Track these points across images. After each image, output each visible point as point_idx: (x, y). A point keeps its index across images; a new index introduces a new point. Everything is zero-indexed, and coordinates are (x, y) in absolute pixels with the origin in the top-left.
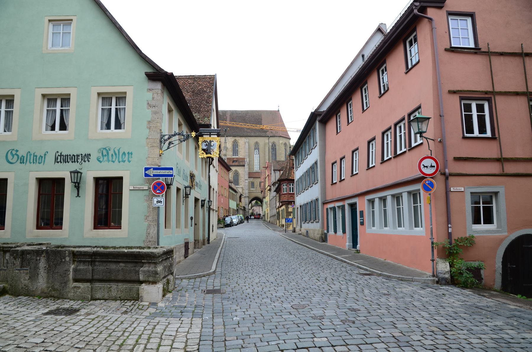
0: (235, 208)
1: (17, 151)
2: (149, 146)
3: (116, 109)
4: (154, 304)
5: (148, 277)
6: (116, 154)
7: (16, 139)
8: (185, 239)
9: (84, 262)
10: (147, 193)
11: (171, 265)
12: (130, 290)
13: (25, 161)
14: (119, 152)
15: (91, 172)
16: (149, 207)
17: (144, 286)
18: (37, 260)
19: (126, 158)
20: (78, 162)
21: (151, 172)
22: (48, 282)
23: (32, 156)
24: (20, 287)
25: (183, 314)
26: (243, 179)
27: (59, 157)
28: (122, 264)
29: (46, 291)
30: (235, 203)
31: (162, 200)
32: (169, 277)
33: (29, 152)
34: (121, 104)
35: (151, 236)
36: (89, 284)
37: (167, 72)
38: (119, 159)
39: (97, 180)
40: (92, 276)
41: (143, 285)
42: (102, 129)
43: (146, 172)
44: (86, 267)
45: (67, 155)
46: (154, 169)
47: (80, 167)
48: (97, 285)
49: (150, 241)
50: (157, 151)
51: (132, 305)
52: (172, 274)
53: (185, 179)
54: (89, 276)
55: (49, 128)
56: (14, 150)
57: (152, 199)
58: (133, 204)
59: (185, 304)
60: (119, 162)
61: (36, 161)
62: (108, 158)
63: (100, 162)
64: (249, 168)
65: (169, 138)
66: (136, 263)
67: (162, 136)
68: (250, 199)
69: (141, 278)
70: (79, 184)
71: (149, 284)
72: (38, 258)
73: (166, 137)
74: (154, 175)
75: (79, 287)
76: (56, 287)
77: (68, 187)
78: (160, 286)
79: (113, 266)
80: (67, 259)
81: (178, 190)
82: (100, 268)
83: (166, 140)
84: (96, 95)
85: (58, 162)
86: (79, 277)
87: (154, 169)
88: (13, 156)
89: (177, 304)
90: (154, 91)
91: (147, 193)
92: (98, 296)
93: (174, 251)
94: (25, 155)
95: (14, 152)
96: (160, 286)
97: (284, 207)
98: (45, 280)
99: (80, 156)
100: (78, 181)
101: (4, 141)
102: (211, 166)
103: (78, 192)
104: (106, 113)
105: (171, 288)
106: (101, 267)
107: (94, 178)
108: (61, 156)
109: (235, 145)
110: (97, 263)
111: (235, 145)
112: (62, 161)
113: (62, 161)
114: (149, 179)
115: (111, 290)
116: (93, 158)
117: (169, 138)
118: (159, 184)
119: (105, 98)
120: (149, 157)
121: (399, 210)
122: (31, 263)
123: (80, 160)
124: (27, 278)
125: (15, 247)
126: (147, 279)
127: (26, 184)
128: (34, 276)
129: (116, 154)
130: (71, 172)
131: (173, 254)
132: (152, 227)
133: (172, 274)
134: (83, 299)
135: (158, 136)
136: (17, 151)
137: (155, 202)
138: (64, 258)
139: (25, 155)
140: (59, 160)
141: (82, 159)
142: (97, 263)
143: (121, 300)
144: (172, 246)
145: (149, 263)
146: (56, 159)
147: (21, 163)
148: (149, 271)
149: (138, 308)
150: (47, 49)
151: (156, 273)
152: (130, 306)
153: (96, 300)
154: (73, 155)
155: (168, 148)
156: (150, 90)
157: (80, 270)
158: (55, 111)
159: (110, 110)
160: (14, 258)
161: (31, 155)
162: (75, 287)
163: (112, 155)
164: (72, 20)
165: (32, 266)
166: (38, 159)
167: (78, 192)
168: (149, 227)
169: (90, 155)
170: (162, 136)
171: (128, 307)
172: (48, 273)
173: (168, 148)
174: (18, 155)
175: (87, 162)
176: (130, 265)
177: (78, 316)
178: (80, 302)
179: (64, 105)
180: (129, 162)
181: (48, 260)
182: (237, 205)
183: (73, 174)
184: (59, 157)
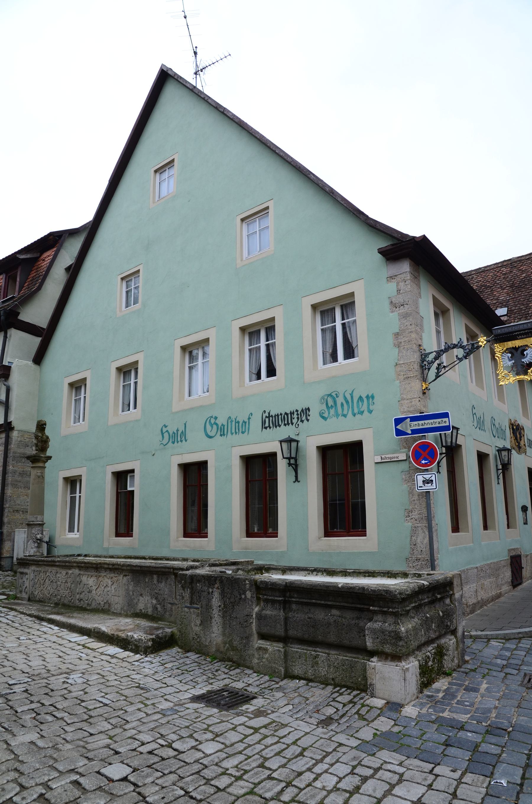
1: (216, 418)
2: (402, 377)
3: (344, 325)
4: (394, 707)
5: (383, 642)
6: (347, 402)
8: (509, 550)
9: (273, 602)
10: (405, 466)
11: (449, 614)
12: (351, 667)
13: (225, 433)
14: (352, 397)
16: (411, 492)
17: (375, 663)
18: (209, 593)
19: (365, 407)
20: (292, 424)
21: (408, 426)
22: (224, 634)
23: (234, 423)
24: (191, 636)
25: (451, 751)
27: (267, 420)
28: (335, 612)
29: (222, 649)
31: (433, 478)
32: (443, 641)
33: (230, 417)
34: (350, 315)
35: (419, 549)
36: (281, 645)
37: (414, 238)
38: (353, 410)
40: (286, 630)
41: (375, 659)
42: (325, 363)
43: (398, 427)
44: (274, 613)
45: (278, 415)
46: (413, 419)
47: (297, 431)
48: (296, 649)
49: (418, 560)
50: (417, 385)
51: (351, 702)
52: (454, 632)
53: (498, 433)
54: (280, 631)
55: (254, 376)
56: (212, 417)
57: (411, 480)
58: (381, 489)
59: (463, 718)
60: (354, 415)
61: (239, 430)
62: (336, 411)
63: (325, 418)
65: (436, 358)
66: (361, 610)
67: (424, 356)
69: (369, 644)
70: (296, 459)
71: (386, 659)
72: (211, 590)
73: (431, 357)
74: (414, 432)
75: (266, 650)
76: (235, 643)
77: (282, 465)
78: (412, 665)
79: (320, 615)
80: (249, 594)
81: (482, 457)
82: (299, 615)
83: (432, 362)
84: (309, 309)
85: (266, 428)
86: (265, 630)
87: (413, 419)
88: (212, 426)
89: (446, 714)
90: (398, 278)
91: (405, 466)
92: (297, 670)
93: (455, 583)
94: (225, 424)
95: (213, 421)
96: (412, 665)
98: (221, 629)
99: (295, 413)
100: (293, 455)
101: (201, 406)
104: (329, 336)
105: (448, 663)
106: (299, 615)
107: (318, 447)
108: (269, 417)
112: (271, 425)
113: (271, 425)
114: (406, 440)
115: (317, 663)
116: (314, 414)
117: (436, 358)
118: (426, 446)
119: (324, 311)
120: (403, 399)
121: (73, 500)
122: (202, 598)
123: (295, 421)
124: (198, 622)
125: (187, 569)
126: (380, 648)
127: (229, 467)
128: (206, 621)
129: (347, 402)
130: (281, 442)
131: (452, 589)
132: (420, 532)
133: (454, 632)
134: (272, 674)
135: (416, 358)
136: (216, 418)
137: (420, 483)
138: (244, 593)
140: (267, 425)
141: (298, 418)
142: (294, 606)
143: (335, 686)
144: (450, 574)
145: (384, 613)
146: (263, 423)
147: (221, 435)
148: (383, 631)
149: (357, 713)
150: (242, 260)
151: (397, 637)
152: (344, 705)
153: (293, 677)
154: (286, 414)
155: (438, 376)
156: (391, 278)
157: (265, 617)
158: (259, 348)
159: (334, 329)
160: (182, 586)
161: (232, 421)
162: (260, 648)
163: (342, 405)
164: (267, 208)
165: (204, 603)
166: (241, 427)
168: (414, 531)
169: (309, 409)
170: (424, 356)
171: (340, 706)
172: (223, 617)
173: (438, 376)
174: (217, 424)
175: (305, 421)
176: (349, 615)
177: (238, 715)
178: (267, 678)
179: (270, 337)
180: (370, 412)
181: (223, 595)
183: (285, 445)
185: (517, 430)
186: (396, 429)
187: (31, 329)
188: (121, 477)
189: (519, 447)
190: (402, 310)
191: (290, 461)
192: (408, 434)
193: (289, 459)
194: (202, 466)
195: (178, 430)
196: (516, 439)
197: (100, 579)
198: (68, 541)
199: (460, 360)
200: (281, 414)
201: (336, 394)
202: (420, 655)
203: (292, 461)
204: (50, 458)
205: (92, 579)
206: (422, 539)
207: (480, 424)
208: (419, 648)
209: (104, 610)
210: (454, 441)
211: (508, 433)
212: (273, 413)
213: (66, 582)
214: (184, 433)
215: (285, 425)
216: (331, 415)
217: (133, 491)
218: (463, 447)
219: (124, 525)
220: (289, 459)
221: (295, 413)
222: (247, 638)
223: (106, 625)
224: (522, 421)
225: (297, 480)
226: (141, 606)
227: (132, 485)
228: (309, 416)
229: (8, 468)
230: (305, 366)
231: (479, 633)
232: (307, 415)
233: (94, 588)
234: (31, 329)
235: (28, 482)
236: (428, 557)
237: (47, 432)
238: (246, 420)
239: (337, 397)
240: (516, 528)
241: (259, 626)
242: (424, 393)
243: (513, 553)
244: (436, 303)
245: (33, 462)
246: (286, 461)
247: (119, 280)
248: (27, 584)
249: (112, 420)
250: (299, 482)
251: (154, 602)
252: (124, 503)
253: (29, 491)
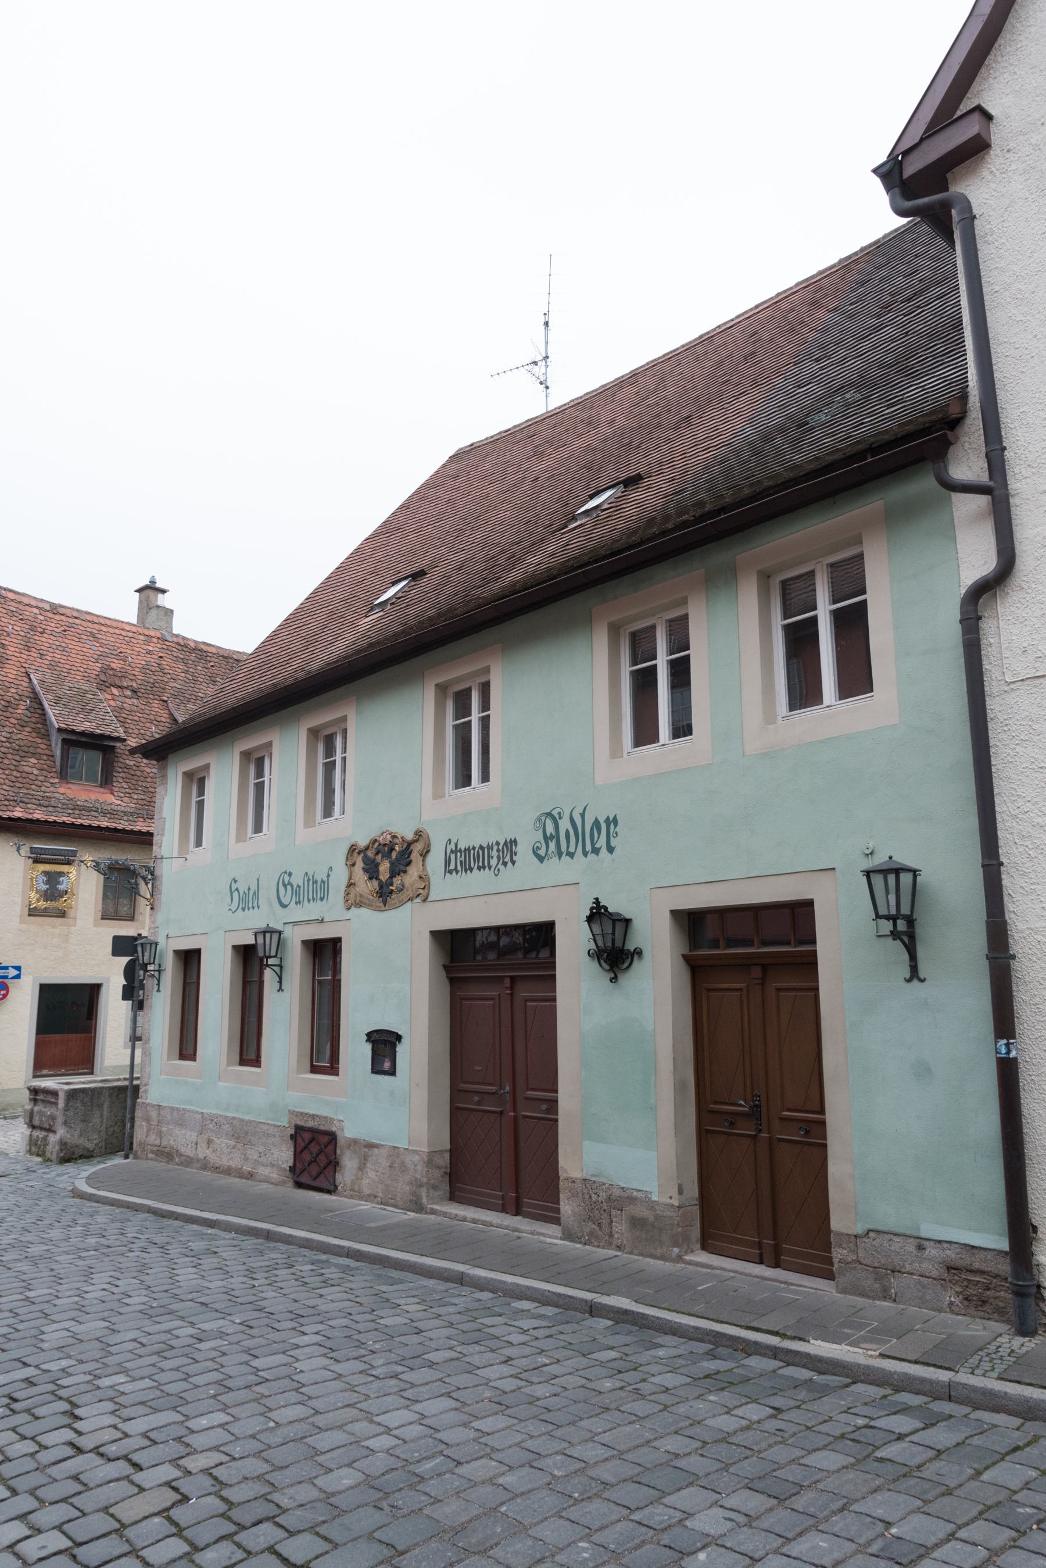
1: (290, 874)
27: (453, 856)
63: (541, 859)
70: (910, 921)
85: (450, 872)
88: (285, 886)
95: (287, 878)
99: (495, 848)
100: (905, 910)
112: (459, 868)
113: (459, 868)
116: (523, 850)
123: (494, 862)
140: (452, 867)
141: (499, 858)
146: (447, 862)
154: (481, 847)
163: (567, 832)
174: (290, 883)
175: (510, 864)
183: (878, 880)
184: (453, 856)
191: (895, 925)
193: (894, 919)
195: (249, 889)
200: (474, 848)
201: (559, 813)
203: (902, 925)
204: (615, 816)
215: (479, 868)
216: (550, 852)
220: (894, 919)
221: (495, 848)
225: (914, 974)
228: (516, 854)
232: (513, 854)
238: (325, 879)
239: (560, 818)
250: (923, 981)
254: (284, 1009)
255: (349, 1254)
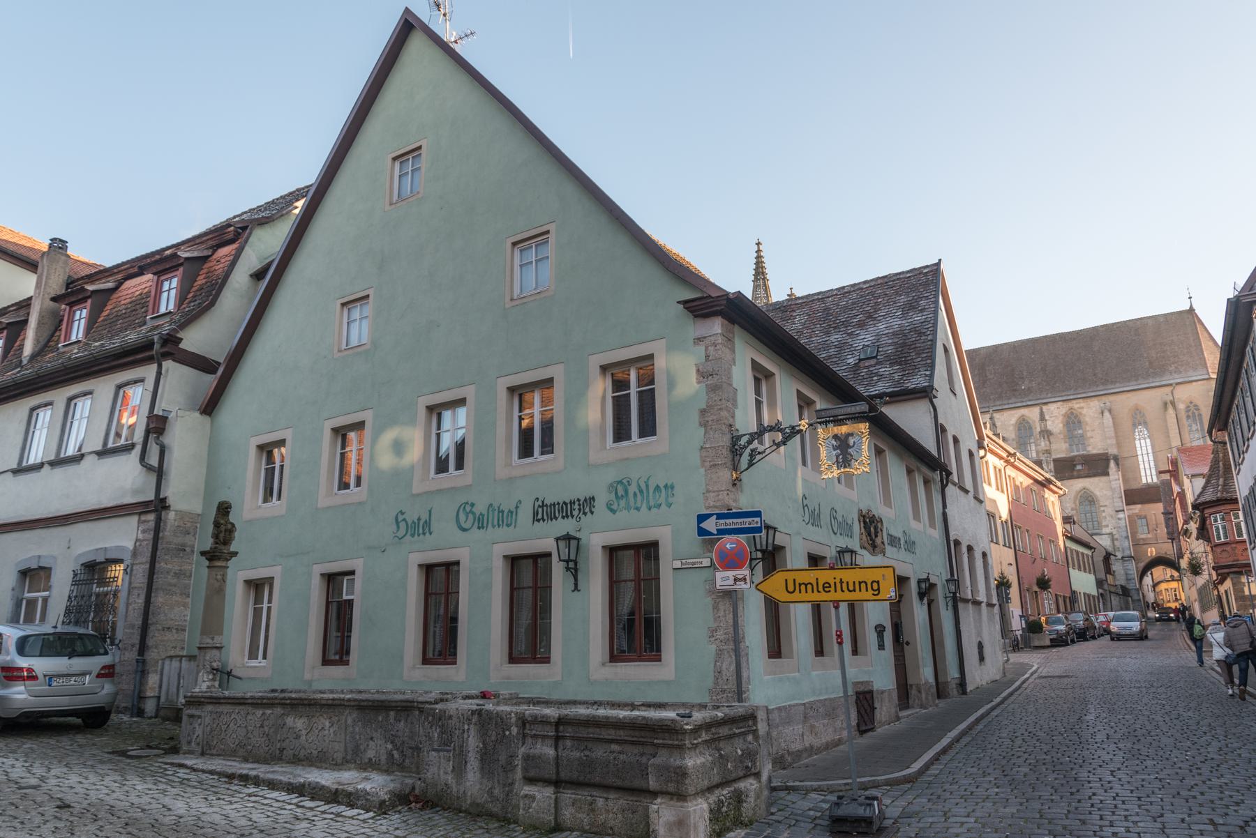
0: (1093, 591)
1: (473, 505)
2: (707, 464)
6: (641, 491)
7: (199, 511)
15: (599, 535)
19: (662, 500)
26: (1109, 511)
30: (1091, 578)
32: (742, 785)
39: (613, 552)
40: (558, 773)
46: (720, 516)
49: (723, 691)
50: (726, 475)
54: (550, 772)
58: (683, 605)
62: (628, 502)
63: (613, 511)
64: (1125, 481)
67: (735, 439)
68: (1142, 565)
69: (653, 784)
73: (743, 441)
75: (533, 798)
85: (538, 521)
86: (532, 774)
87: (720, 516)
90: (707, 341)
94: (485, 512)
97: (1228, 584)
100: (572, 557)
102: (951, 490)
103: (576, 580)
108: (543, 506)
109: (1073, 422)
110: (568, 743)
111: (1073, 422)
116: (600, 505)
120: (708, 491)
123: (575, 513)
129: (641, 491)
130: (557, 539)
131: (755, 724)
135: (726, 440)
136: (473, 505)
138: (509, 730)
139: (485, 512)
140: (540, 516)
142: (568, 743)
146: (535, 514)
151: (682, 773)
154: (565, 503)
155: (751, 464)
163: (635, 494)
164: (548, 232)
166: (505, 517)
167: (576, 580)
168: (719, 654)
170: (735, 439)
173: (751, 464)
174: (474, 514)
182: (1100, 583)
183: (562, 544)
185: (871, 524)
186: (699, 528)
187: (201, 364)
188: (332, 580)
189: (874, 546)
190: (710, 381)
192: (711, 534)
193: (567, 562)
194: (451, 567)
195: (419, 519)
196: (869, 534)
197: (314, 720)
198: (256, 673)
199: (778, 445)
202: (713, 798)
203: (571, 565)
204: (235, 554)
205: (302, 721)
206: (728, 666)
207: (814, 518)
208: (710, 789)
209: (320, 760)
210: (770, 541)
211: (857, 528)
212: (547, 502)
213: (262, 726)
214: (428, 524)
217: (350, 602)
218: (788, 550)
219: (336, 650)
220: (567, 562)
222: (512, 784)
223: (326, 778)
224: (880, 510)
225: (576, 588)
226: (371, 754)
227: (351, 592)
229: (157, 565)
230: (587, 451)
231: (797, 783)
232: (592, 507)
233: (304, 732)
234: (201, 364)
235: (187, 587)
236: (734, 688)
237: (232, 518)
240: (865, 654)
241: (525, 770)
242: (734, 485)
243: (862, 689)
244: (755, 366)
245: (210, 560)
246: (562, 564)
247: (339, 306)
248: (199, 731)
249: (323, 502)
251: (390, 746)
252: (339, 616)
253: (189, 600)
254: (582, 613)
255: (936, 758)
